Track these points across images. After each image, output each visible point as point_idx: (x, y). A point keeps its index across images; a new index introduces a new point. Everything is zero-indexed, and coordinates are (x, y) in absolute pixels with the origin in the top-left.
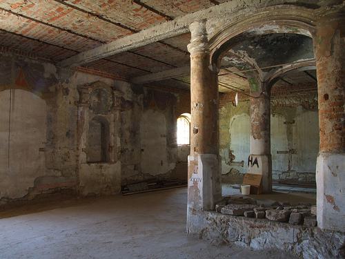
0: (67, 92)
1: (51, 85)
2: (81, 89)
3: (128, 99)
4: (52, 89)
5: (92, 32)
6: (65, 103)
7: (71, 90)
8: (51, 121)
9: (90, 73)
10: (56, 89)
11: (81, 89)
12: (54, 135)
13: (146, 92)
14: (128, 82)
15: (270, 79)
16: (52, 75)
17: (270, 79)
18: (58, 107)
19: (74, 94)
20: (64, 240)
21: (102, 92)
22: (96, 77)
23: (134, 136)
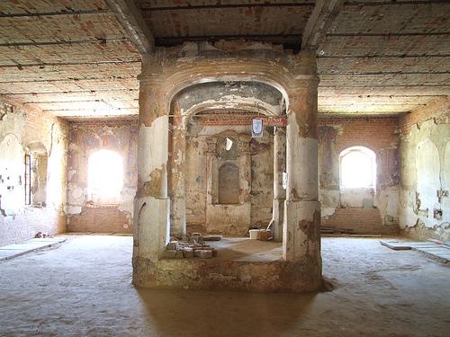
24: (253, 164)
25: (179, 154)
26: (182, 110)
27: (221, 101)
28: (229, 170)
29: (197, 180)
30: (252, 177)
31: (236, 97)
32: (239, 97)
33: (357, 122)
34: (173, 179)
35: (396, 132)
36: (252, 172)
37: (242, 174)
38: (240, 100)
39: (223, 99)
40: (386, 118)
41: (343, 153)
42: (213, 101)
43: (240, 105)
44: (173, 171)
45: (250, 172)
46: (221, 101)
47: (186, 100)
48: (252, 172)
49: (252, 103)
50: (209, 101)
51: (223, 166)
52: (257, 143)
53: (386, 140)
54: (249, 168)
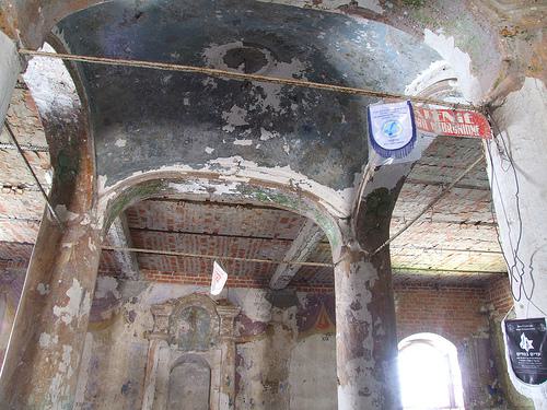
0: (132, 317)
1: (105, 308)
2: (155, 311)
3: (258, 320)
4: (106, 315)
5: (423, 296)
6: (126, 335)
7: (139, 314)
8: (97, 367)
9: (179, 283)
10: (113, 315)
11: (155, 311)
12: (99, 391)
13: (303, 302)
14: (74, 185)
15: (357, 204)
16: (110, 293)
17: (357, 204)
18: (113, 343)
19: (143, 319)
20: (87, 354)
21: (199, 312)
22: (190, 286)
23: (274, 390)
24: (238, 360)
25: (74, 291)
26: (103, 180)
27: (206, 169)
28: (191, 371)
29: (125, 389)
30: (237, 388)
31: (244, 163)
32: (252, 165)
33: (420, 291)
34: (40, 367)
35: (483, 309)
36: (238, 377)
37: (217, 380)
38: (252, 171)
39: (212, 167)
40: (465, 285)
41: (401, 344)
42: (186, 168)
43: (255, 184)
44: (47, 340)
45: (233, 376)
46: (206, 169)
47: (116, 151)
48: (238, 377)
49: (284, 181)
50: (176, 168)
51: (179, 363)
52: (247, 322)
53: (470, 323)
54: (231, 368)
